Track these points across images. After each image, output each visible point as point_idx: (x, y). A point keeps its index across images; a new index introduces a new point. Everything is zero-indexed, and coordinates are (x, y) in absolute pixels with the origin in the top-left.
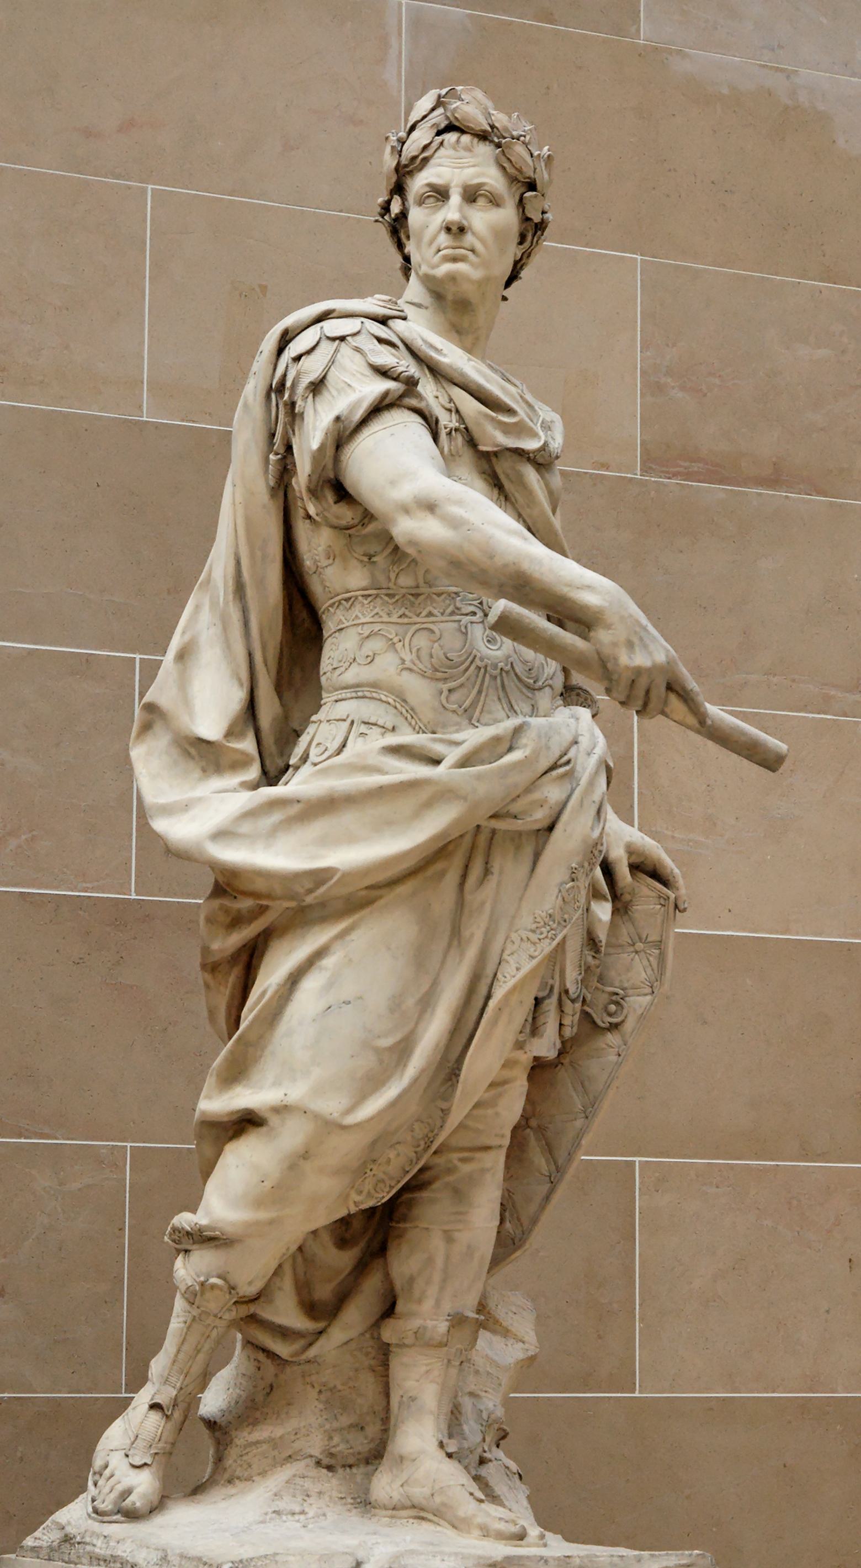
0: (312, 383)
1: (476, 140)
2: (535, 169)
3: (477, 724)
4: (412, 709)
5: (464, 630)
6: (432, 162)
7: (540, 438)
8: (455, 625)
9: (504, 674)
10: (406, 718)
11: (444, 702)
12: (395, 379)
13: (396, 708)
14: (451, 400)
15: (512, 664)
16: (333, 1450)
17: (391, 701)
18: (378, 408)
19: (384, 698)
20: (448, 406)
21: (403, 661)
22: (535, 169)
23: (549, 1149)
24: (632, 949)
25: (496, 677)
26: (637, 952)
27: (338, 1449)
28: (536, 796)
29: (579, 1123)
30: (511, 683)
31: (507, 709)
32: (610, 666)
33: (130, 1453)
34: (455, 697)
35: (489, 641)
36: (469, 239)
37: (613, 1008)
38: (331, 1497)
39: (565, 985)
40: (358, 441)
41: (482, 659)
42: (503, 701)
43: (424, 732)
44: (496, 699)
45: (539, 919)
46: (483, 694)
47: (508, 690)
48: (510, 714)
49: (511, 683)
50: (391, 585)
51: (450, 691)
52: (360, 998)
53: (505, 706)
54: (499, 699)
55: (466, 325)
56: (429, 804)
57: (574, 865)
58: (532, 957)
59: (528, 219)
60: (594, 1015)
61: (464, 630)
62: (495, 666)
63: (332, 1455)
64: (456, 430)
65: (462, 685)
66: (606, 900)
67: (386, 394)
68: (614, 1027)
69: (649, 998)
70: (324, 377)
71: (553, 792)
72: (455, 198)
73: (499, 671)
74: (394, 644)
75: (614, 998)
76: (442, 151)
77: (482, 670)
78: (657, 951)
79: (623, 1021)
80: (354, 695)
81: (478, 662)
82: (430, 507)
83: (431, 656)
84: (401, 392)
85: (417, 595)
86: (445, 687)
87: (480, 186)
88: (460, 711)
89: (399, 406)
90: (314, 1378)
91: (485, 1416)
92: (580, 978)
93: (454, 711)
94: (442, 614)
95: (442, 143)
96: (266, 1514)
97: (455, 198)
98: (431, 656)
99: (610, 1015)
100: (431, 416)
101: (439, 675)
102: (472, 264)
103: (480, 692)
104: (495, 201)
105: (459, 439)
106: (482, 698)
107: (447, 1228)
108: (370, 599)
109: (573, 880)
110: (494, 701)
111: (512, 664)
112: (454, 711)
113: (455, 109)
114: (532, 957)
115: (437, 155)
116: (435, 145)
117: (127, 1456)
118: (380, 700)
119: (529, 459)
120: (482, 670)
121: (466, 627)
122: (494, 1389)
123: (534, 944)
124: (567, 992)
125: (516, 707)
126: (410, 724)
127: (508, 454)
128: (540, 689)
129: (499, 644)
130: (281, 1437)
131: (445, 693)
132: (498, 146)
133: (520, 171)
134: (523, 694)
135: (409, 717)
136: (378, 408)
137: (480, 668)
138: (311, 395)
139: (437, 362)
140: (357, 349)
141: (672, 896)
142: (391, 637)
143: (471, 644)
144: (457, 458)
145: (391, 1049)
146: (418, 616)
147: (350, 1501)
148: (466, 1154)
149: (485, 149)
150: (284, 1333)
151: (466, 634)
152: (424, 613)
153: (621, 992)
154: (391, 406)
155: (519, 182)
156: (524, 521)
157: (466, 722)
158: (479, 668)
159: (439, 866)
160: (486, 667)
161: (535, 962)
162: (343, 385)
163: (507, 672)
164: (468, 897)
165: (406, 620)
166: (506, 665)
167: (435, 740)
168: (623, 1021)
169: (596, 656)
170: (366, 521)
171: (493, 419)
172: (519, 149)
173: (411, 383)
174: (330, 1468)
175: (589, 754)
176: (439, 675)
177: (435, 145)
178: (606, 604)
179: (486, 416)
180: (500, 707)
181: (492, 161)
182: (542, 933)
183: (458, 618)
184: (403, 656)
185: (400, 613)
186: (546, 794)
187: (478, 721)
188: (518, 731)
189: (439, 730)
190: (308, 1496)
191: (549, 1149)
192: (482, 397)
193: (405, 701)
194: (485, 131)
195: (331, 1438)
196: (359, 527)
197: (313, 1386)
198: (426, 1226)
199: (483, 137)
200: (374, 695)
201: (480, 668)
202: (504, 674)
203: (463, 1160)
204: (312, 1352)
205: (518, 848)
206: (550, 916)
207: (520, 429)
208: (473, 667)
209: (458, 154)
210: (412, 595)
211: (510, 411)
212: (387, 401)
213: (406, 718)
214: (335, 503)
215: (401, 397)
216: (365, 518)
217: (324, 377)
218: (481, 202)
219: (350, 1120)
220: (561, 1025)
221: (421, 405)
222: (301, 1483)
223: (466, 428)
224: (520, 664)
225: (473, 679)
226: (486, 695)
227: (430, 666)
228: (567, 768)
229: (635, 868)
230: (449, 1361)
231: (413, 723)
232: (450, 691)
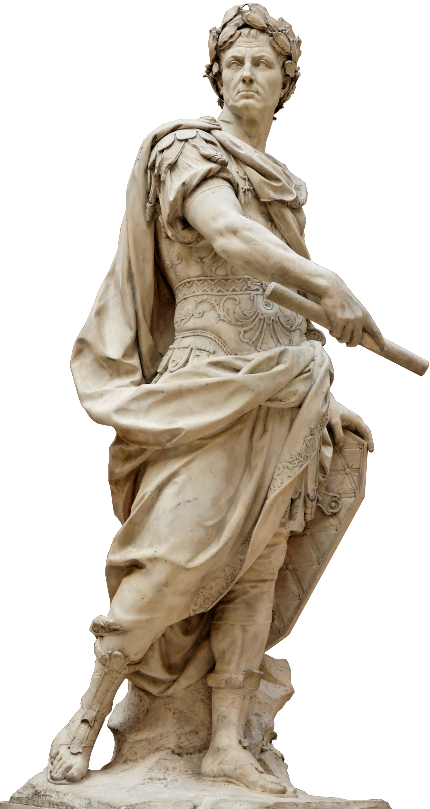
0: (170, 165)
1: (259, 32)
2: (291, 48)
3: (259, 350)
4: (224, 342)
5: (252, 299)
6: (235, 44)
7: (294, 194)
8: (248, 296)
9: (274, 323)
10: (221, 347)
11: (242, 338)
12: (215, 162)
13: (215, 341)
14: (245, 174)
15: (278, 317)
16: (181, 745)
17: (212, 337)
18: (206, 178)
19: (209, 336)
20: (244, 177)
21: (219, 316)
22: (291, 48)
23: (299, 581)
24: (344, 472)
25: (270, 325)
26: (346, 474)
27: (184, 744)
28: (292, 389)
29: (315, 567)
30: (278, 328)
31: (276, 342)
32: (331, 318)
33: (71, 746)
34: (247, 335)
35: (266, 305)
36: (255, 86)
37: (333, 504)
38: (180, 770)
39: (307, 492)
40: (195, 196)
41: (262, 315)
42: (274, 337)
43: (231, 354)
44: (270, 336)
45: (293, 456)
46: (263, 334)
47: (277, 332)
48: (277, 345)
49: (278, 328)
50: (213, 274)
51: (245, 332)
52: (196, 499)
53: (275, 340)
54: (272, 336)
55: (253, 133)
56: (233, 394)
57: (312, 427)
58: (290, 477)
59: (287, 75)
60: (323, 508)
61: (252, 299)
62: (269, 319)
63: (180, 748)
64: (248, 190)
65: (251, 329)
66: (330, 445)
67: (210, 170)
68: (334, 515)
69: (353, 499)
70: (176, 161)
71: (301, 387)
72: (248, 64)
73: (271, 321)
74: (215, 306)
75: (334, 499)
76: (241, 38)
77: (262, 321)
78: (358, 474)
79: (339, 512)
80: (192, 334)
81: (260, 316)
82: (234, 232)
83: (235, 313)
84: (218, 169)
85: (227, 280)
86: (242, 330)
87: (261, 57)
88: (251, 343)
89: (217, 177)
90: (171, 706)
91: (264, 726)
92: (315, 488)
93: (247, 343)
94: (241, 290)
95: (240, 34)
96: (145, 780)
97: (248, 64)
98: (235, 313)
99: (332, 508)
100: (235, 182)
101: (239, 323)
102: (257, 100)
103: (261, 333)
104: (269, 66)
105: (250, 195)
106: (262, 336)
107: (243, 624)
108: (201, 282)
109: (312, 435)
110: (269, 337)
111: (278, 317)
112: (247, 343)
113: (248, 16)
114: (290, 477)
115: (238, 40)
116: (236, 35)
117: (69, 748)
118: (207, 337)
119: (288, 206)
120: (262, 321)
121: (253, 297)
122: (269, 712)
123: (291, 469)
124: (308, 496)
125: (281, 341)
126: (223, 350)
127: (276, 203)
128: (294, 331)
129: (271, 306)
130: (153, 738)
131: (242, 333)
132: (271, 35)
133: (283, 49)
134: (285, 333)
135: (223, 346)
136: (206, 178)
137: (261, 320)
138: (169, 171)
139: (238, 153)
140: (194, 146)
141: (366, 443)
142: (213, 302)
143: (256, 306)
144: (249, 205)
145: (212, 527)
146: (227, 291)
147: (190, 772)
148: (253, 584)
149: (264, 38)
150: (155, 681)
151: (253, 301)
152: (231, 290)
153: (338, 496)
154: (212, 177)
155: (282, 55)
156: (285, 240)
157: (253, 349)
158: (260, 320)
159: (239, 427)
160: (264, 319)
161: (291, 479)
162: (187, 165)
163: (276, 322)
164: (255, 444)
165: (221, 294)
166: (276, 318)
167: (237, 359)
168: (339, 512)
169: (324, 313)
170: (199, 239)
171: (268, 184)
172: (283, 37)
173: (224, 165)
174: (179, 755)
175: (320, 366)
176: (239, 323)
177: (236, 35)
178: (330, 285)
179: (265, 182)
180: (272, 341)
181: (268, 44)
182: (295, 464)
183: (249, 292)
184: (219, 313)
185: (218, 289)
186: (297, 388)
187: (260, 349)
188: (282, 354)
189: (239, 353)
190: (168, 770)
191: (299, 581)
192: (262, 172)
193: (220, 337)
194: (264, 28)
195: (180, 738)
196: (195, 243)
197: (170, 710)
198: (232, 623)
199: (263, 30)
200: (204, 334)
201: (261, 320)
202: (274, 323)
203: (252, 587)
204: (170, 692)
205: (282, 417)
206: (299, 454)
207: (283, 190)
208: (257, 319)
209: (249, 40)
210: (224, 280)
211: (277, 180)
212: (211, 174)
213: (221, 347)
214: (182, 230)
215: (218, 172)
216: (198, 238)
217: (176, 161)
218: (262, 66)
219: (191, 565)
220: (305, 513)
221: (229, 177)
222: (164, 763)
223: (254, 189)
224: (283, 317)
225: (257, 326)
226: (265, 334)
227: (234, 319)
228: (309, 374)
229: (345, 428)
230: (244, 696)
231: (225, 349)
232: (245, 332)
